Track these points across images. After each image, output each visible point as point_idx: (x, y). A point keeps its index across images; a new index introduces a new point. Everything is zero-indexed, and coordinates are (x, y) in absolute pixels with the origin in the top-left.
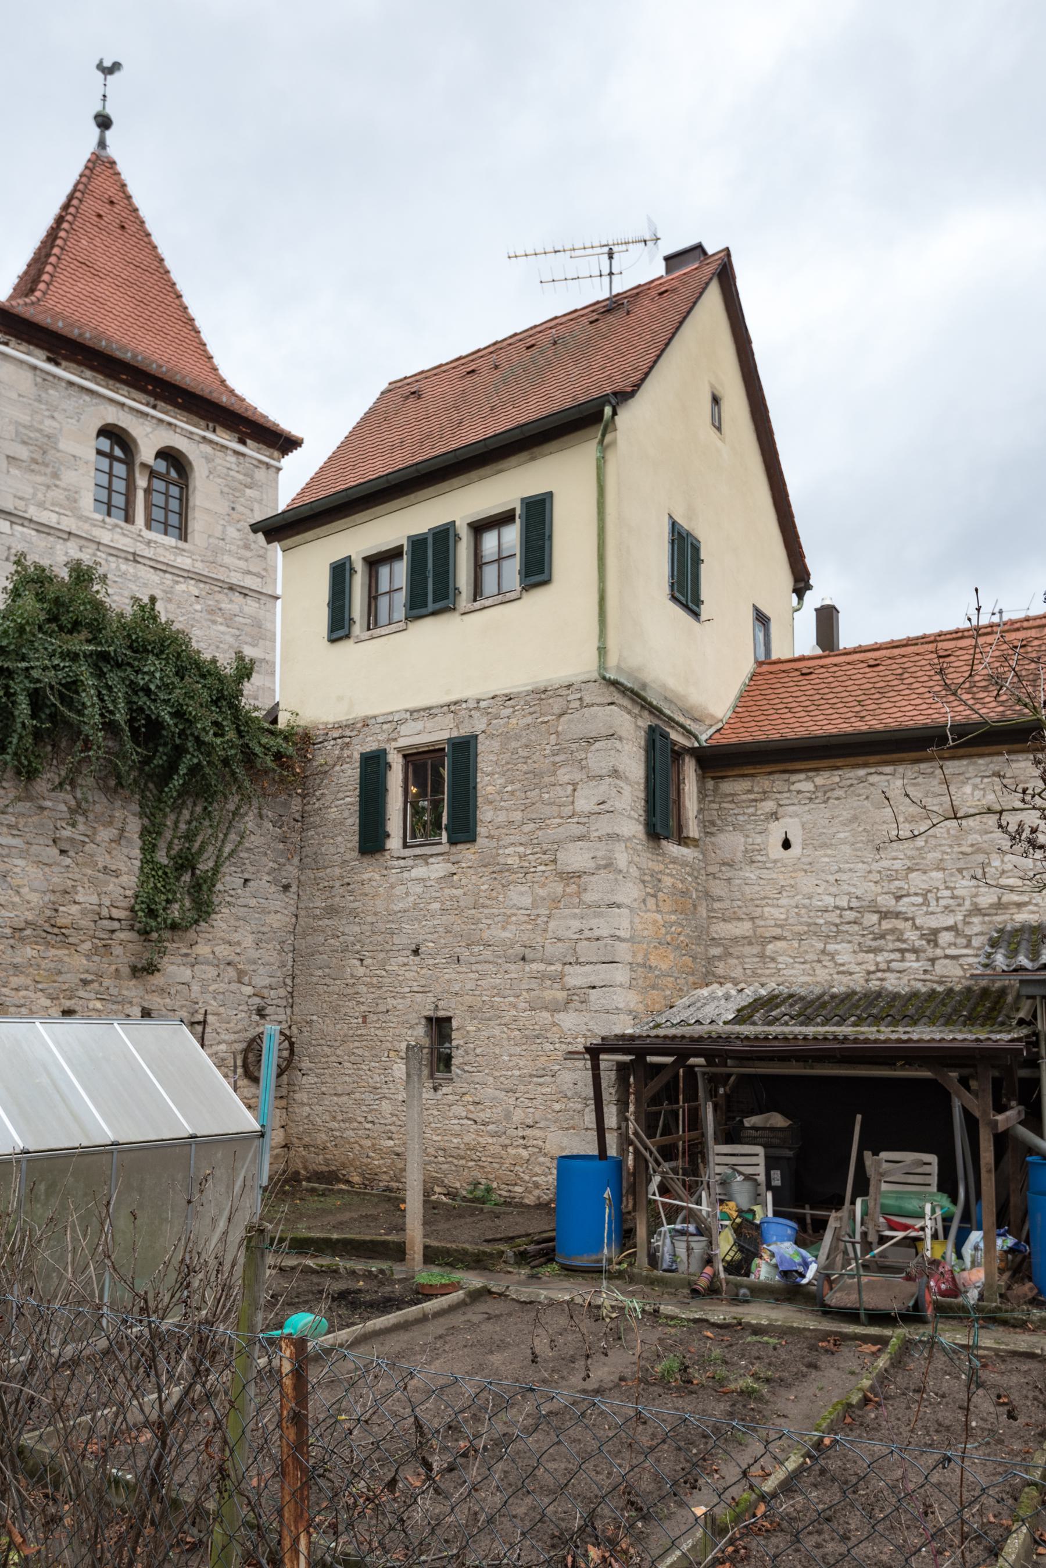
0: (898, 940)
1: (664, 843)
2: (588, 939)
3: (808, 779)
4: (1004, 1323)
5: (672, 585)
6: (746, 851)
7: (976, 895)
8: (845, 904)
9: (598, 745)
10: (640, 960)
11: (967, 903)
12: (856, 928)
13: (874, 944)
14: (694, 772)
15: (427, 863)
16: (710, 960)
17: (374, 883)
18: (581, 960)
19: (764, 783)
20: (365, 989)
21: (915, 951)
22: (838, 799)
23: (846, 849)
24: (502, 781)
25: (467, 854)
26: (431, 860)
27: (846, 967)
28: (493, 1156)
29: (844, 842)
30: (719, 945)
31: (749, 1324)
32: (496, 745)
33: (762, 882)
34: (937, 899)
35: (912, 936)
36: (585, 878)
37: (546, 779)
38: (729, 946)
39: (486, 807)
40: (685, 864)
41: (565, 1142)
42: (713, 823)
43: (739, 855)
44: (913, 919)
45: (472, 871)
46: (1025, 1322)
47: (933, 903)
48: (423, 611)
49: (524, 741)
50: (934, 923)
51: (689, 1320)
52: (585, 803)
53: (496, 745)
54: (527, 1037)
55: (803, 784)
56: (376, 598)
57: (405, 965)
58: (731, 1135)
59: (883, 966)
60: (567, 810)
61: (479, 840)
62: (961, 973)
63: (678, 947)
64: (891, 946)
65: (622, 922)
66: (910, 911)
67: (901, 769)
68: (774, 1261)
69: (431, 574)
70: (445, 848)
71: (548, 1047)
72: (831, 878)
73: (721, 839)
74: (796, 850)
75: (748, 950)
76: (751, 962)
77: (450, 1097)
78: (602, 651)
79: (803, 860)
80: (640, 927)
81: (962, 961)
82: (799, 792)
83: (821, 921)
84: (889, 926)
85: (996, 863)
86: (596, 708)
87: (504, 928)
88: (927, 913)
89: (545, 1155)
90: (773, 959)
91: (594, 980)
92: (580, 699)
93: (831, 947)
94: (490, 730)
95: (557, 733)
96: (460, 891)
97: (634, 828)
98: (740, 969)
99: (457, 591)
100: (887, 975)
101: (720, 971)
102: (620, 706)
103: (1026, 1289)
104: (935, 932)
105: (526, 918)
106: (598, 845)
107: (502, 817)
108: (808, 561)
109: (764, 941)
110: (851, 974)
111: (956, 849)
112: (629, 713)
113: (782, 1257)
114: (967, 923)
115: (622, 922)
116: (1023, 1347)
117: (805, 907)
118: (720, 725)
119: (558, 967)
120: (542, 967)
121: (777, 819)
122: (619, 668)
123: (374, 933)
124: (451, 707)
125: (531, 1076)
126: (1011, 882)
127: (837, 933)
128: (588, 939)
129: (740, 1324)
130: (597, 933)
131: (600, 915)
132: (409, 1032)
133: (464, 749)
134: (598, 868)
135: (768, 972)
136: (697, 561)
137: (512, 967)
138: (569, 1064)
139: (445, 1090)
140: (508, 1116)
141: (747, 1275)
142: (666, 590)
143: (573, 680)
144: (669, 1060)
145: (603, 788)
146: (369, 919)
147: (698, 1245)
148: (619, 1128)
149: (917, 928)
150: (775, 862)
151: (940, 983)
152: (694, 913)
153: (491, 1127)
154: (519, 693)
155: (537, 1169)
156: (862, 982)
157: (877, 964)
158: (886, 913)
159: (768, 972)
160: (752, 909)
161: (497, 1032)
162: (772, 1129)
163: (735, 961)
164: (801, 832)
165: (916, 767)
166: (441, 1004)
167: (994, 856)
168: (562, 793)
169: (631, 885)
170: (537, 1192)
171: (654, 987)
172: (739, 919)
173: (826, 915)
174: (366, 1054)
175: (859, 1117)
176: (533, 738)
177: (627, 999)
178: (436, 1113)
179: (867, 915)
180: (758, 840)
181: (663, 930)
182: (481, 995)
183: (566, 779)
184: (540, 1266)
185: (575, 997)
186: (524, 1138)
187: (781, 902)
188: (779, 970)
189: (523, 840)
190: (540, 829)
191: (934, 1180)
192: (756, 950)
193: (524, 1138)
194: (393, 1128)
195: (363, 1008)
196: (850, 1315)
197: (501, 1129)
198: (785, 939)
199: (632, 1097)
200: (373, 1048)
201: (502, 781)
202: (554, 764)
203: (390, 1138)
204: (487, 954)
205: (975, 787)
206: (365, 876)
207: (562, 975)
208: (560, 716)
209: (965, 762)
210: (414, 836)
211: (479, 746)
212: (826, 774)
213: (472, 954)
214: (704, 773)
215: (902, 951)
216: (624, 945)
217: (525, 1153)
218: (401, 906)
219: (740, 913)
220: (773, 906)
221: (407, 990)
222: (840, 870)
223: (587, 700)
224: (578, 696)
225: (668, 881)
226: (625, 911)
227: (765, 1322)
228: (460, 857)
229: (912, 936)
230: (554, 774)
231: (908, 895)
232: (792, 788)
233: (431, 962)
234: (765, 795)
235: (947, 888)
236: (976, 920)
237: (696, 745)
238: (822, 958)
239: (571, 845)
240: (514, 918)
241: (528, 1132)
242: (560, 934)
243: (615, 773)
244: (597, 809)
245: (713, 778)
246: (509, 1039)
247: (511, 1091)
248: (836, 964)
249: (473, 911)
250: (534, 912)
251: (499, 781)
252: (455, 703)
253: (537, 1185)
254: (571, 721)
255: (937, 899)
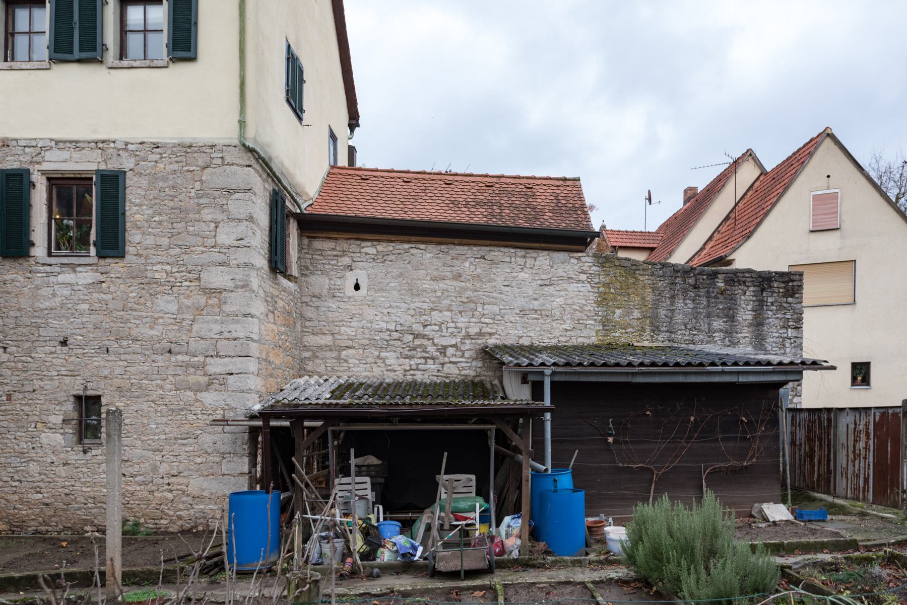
0: (424, 351)
1: (279, 276)
2: (228, 339)
3: (373, 246)
4: (533, 566)
5: (287, 91)
6: (330, 289)
7: (468, 327)
8: (393, 328)
9: (237, 195)
10: (264, 357)
11: (463, 331)
12: (399, 343)
13: (409, 353)
14: (305, 229)
15: (75, 271)
16: (303, 360)
17: (18, 284)
18: (220, 354)
19: (344, 245)
20: (9, 372)
21: (433, 358)
22: (391, 261)
23: (395, 293)
24: (150, 212)
25: (115, 267)
26: (79, 269)
27: (389, 367)
28: (140, 499)
29: (394, 289)
30: (309, 350)
31: (399, 591)
32: (144, 182)
33: (340, 310)
34: (447, 328)
35: (432, 349)
36: (224, 294)
37: (191, 216)
38: (316, 352)
39: (134, 231)
40: (290, 294)
41: (205, 485)
42: (307, 268)
43: (325, 292)
44: (433, 339)
45: (120, 281)
46: (544, 564)
47: (445, 330)
48: (69, 57)
49: (171, 183)
50: (444, 342)
51: (356, 595)
52: (225, 236)
53: (144, 182)
54: (172, 410)
55: (369, 249)
56: (13, 35)
57: (52, 353)
58: (345, 471)
59: (414, 367)
60: (210, 242)
61: (127, 256)
62: (458, 372)
63: (285, 350)
64: (419, 355)
65: (254, 328)
66: (431, 334)
67: (430, 247)
68: (395, 548)
69: (77, 26)
70: (95, 260)
71: (191, 417)
72: (385, 311)
73: (312, 279)
74: (363, 291)
75: (329, 354)
76: (331, 362)
77: (100, 457)
78: (242, 123)
79: (368, 298)
80: (265, 333)
81: (459, 365)
82: (366, 254)
83: (378, 338)
84: (419, 343)
85: (480, 309)
86: (235, 167)
87: (151, 328)
88: (441, 336)
89: (188, 495)
90: (346, 361)
91: (231, 368)
92: (222, 158)
93: (383, 355)
94: (137, 169)
95: (201, 181)
96: (109, 297)
97: (261, 262)
98: (323, 367)
99: (104, 48)
100: (416, 372)
101: (309, 368)
102: (255, 169)
103: (542, 545)
104: (445, 348)
105: (172, 321)
106: (237, 270)
107: (150, 241)
108: (359, 106)
109: (341, 349)
110: (395, 371)
111: (459, 299)
112: (260, 176)
113: (400, 545)
114: (462, 343)
115: (254, 328)
116: (563, 579)
117: (368, 328)
118: (311, 202)
119: (201, 359)
120: (186, 358)
121: (351, 270)
122: (255, 140)
123: (18, 326)
124: (99, 144)
125: (176, 439)
126: (487, 320)
127: (387, 346)
128: (228, 339)
129: (392, 592)
130: (234, 335)
131: (238, 322)
132: (58, 408)
133: (112, 183)
134: (237, 287)
135: (342, 369)
136: (302, 81)
137: (160, 358)
138: (210, 429)
139: (94, 452)
140: (155, 469)
141: (374, 559)
142: (283, 94)
143: (216, 142)
144: (319, 424)
145: (242, 228)
146: (12, 314)
147: (339, 544)
148: (250, 472)
149: (435, 345)
150: (349, 298)
151: (447, 378)
152: (294, 328)
153: (139, 478)
154: (165, 144)
155: (181, 506)
156: (401, 376)
157: (411, 366)
158: (417, 335)
159: (342, 369)
160: (332, 327)
161: (145, 406)
162: (369, 466)
163: (320, 361)
164: (367, 280)
165: (439, 247)
166: (90, 385)
167: (479, 305)
168: (206, 228)
169: (259, 302)
170: (180, 523)
171: (271, 376)
172: (324, 334)
173: (381, 334)
174: (12, 425)
175: (446, 454)
176: (179, 181)
177: (256, 383)
178: (85, 470)
179: (406, 336)
180: (338, 283)
181: (277, 337)
182: (129, 379)
183: (209, 217)
184: (216, 574)
185: (215, 381)
186: (169, 484)
187: (353, 324)
188: (349, 368)
189: (170, 260)
190: (186, 253)
191: (474, 490)
192: (334, 354)
193: (169, 484)
194: (41, 484)
195: (7, 388)
196: (454, 575)
197: (149, 478)
198: (354, 348)
199: (260, 451)
200: (18, 420)
201: (150, 212)
202: (199, 205)
203: (39, 492)
204: (136, 347)
205: (471, 263)
206: (8, 277)
207: (204, 365)
208: (204, 168)
209: (466, 248)
210: (58, 248)
211: (127, 181)
212: (385, 244)
213: (120, 346)
214: (302, 232)
215: (426, 358)
216: (255, 345)
217: (170, 496)
218: (47, 304)
219: (325, 330)
220: (347, 326)
221: (56, 373)
222: (390, 307)
223: (228, 159)
224: (221, 155)
225: (281, 303)
226: (255, 320)
227: (409, 588)
228: (109, 268)
229: (432, 349)
230: (199, 212)
231: (431, 325)
232: (362, 250)
233: (80, 351)
234: (344, 253)
235: (453, 322)
236: (467, 341)
237: (298, 211)
238: (377, 361)
239: (213, 268)
240: (161, 320)
241: (173, 480)
242: (203, 334)
243: (251, 219)
244: (236, 243)
245: (308, 237)
246: (156, 412)
247: (158, 450)
248: (386, 365)
249: (122, 313)
250: (180, 316)
251: (147, 212)
252: (103, 142)
253: (180, 518)
254: (214, 174)
255: (447, 328)
